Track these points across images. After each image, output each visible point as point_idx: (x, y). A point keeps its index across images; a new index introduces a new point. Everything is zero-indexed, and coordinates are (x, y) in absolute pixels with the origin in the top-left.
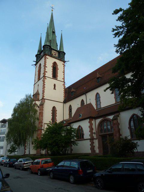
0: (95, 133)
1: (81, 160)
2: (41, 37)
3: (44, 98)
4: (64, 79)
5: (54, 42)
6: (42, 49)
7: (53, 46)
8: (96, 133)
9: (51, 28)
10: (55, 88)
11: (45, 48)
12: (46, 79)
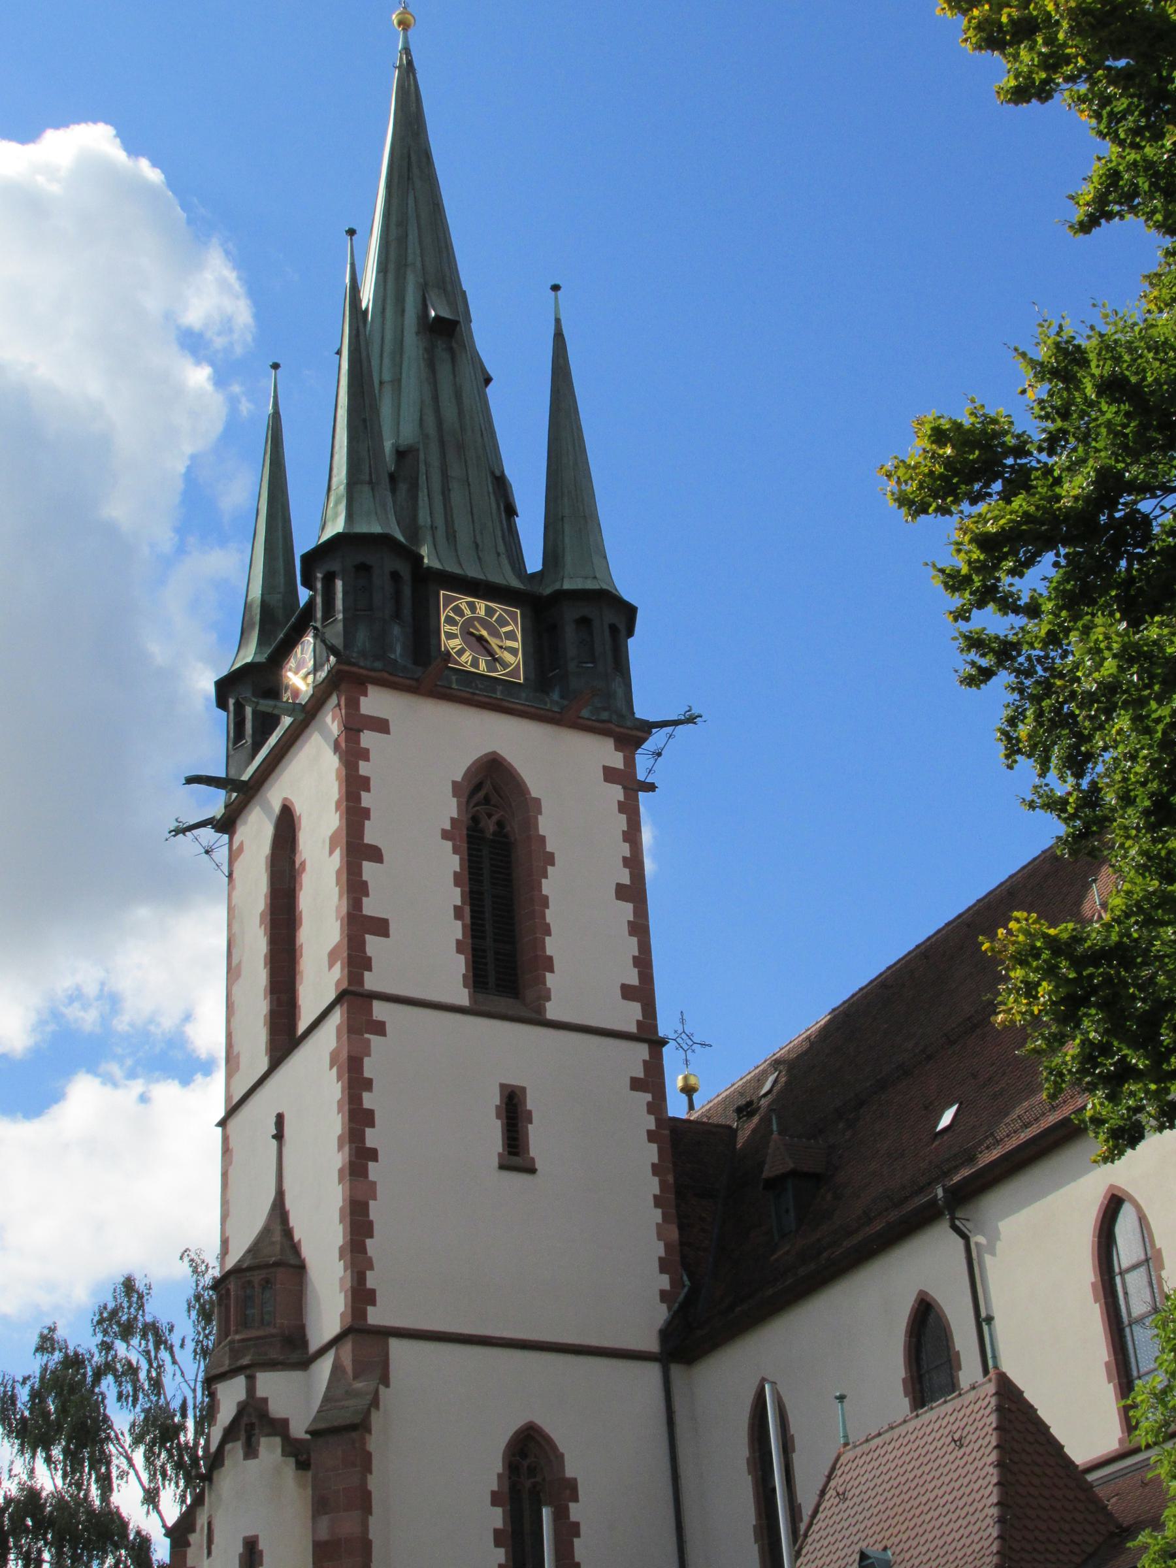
1: (421, 447)
2: (559, 337)
3: (375, 1316)
5: (455, 471)
7: (451, 536)
11: (329, 580)
12: (379, 1028)
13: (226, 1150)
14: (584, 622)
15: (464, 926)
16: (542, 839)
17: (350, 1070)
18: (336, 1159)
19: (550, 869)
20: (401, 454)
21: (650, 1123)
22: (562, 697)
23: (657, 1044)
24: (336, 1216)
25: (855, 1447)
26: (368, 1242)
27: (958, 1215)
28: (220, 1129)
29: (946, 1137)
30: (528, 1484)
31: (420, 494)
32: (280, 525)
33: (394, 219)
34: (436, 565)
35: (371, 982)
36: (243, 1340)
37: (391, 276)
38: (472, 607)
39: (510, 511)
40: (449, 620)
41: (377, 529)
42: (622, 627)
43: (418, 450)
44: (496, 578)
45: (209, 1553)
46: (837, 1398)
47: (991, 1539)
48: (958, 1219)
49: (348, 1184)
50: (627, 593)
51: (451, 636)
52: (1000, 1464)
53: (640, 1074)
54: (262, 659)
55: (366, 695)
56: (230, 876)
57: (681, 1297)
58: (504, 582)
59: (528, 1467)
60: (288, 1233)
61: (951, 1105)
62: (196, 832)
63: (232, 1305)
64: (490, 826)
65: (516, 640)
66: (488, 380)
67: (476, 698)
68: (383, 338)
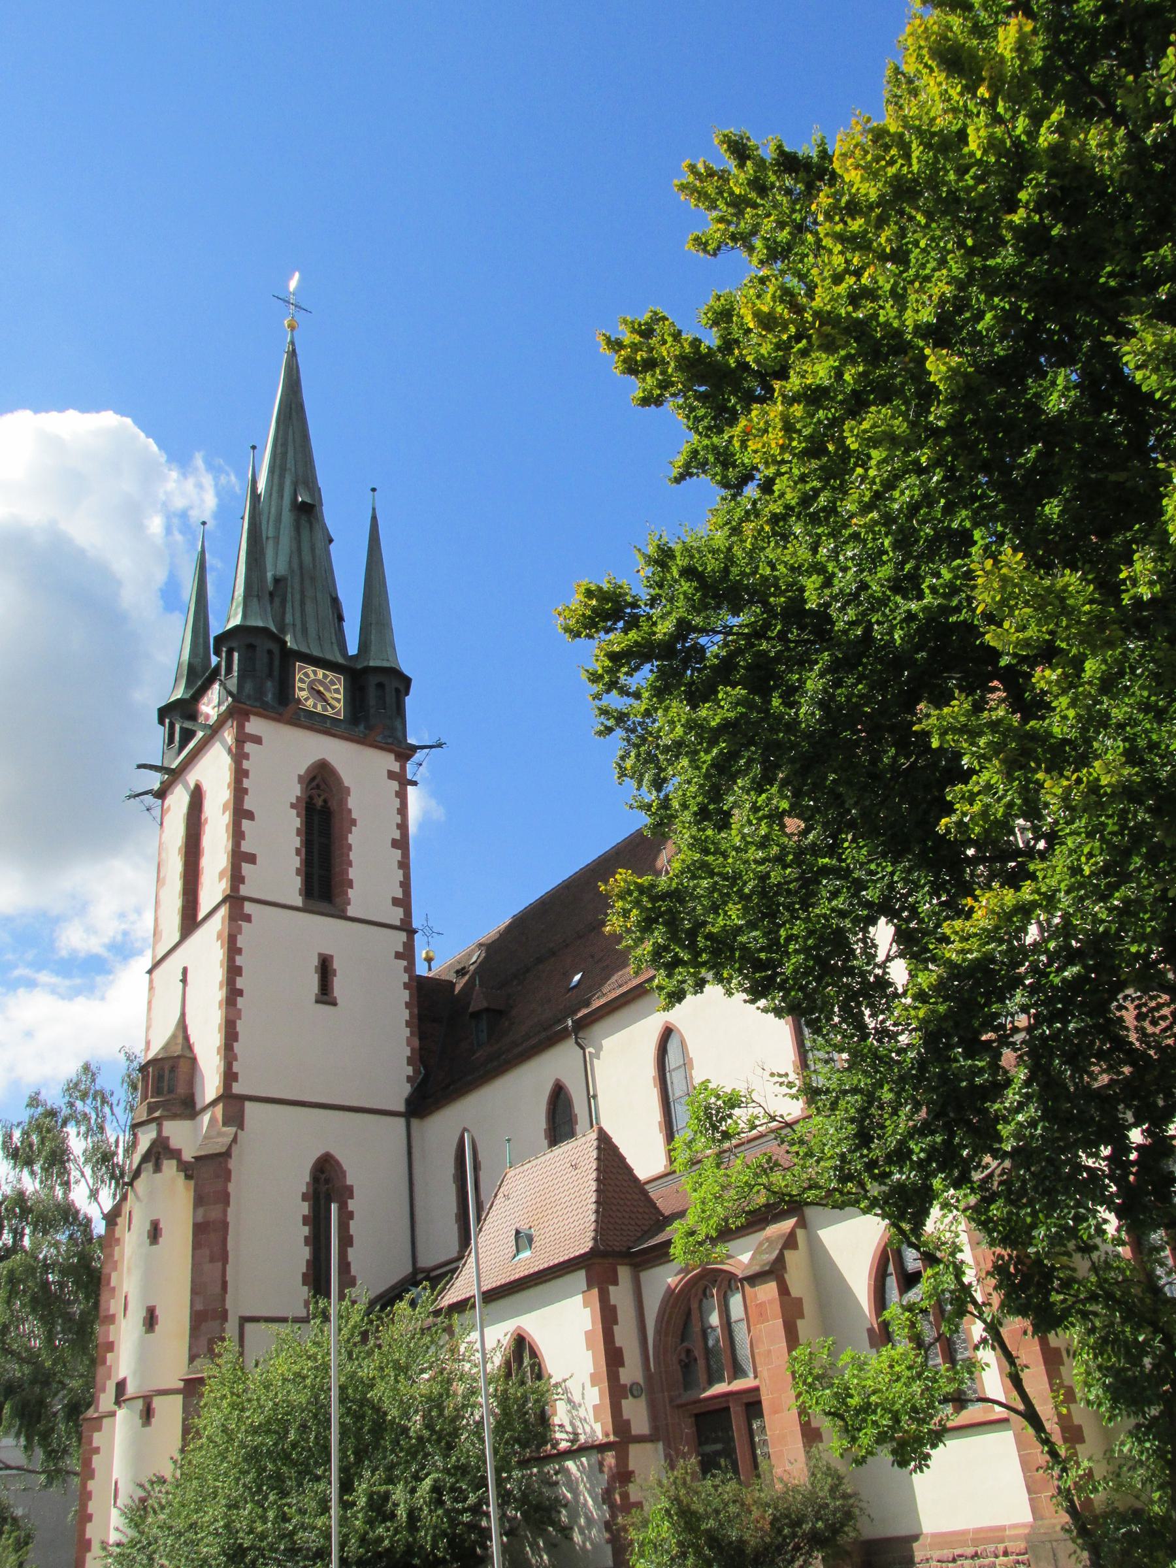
3: (237, 1088)
4: (404, 902)
7: (305, 630)
8: (651, 1388)
10: (325, 994)
12: (248, 918)
13: (151, 988)
14: (380, 686)
16: (350, 811)
18: (219, 995)
23: (411, 932)
33: (280, 442)
35: (244, 891)
38: (315, 673)
39: (341, 618)
40: (301, 681)
41: (260, 624)
42: (402, 688)
44: (329, 657)
50: (406, 670)
51: (301, 689)
52: (598, 1180)
53: (401, 950)
60: (186, 1038)
64: (319, 802)
66: (331, 541)
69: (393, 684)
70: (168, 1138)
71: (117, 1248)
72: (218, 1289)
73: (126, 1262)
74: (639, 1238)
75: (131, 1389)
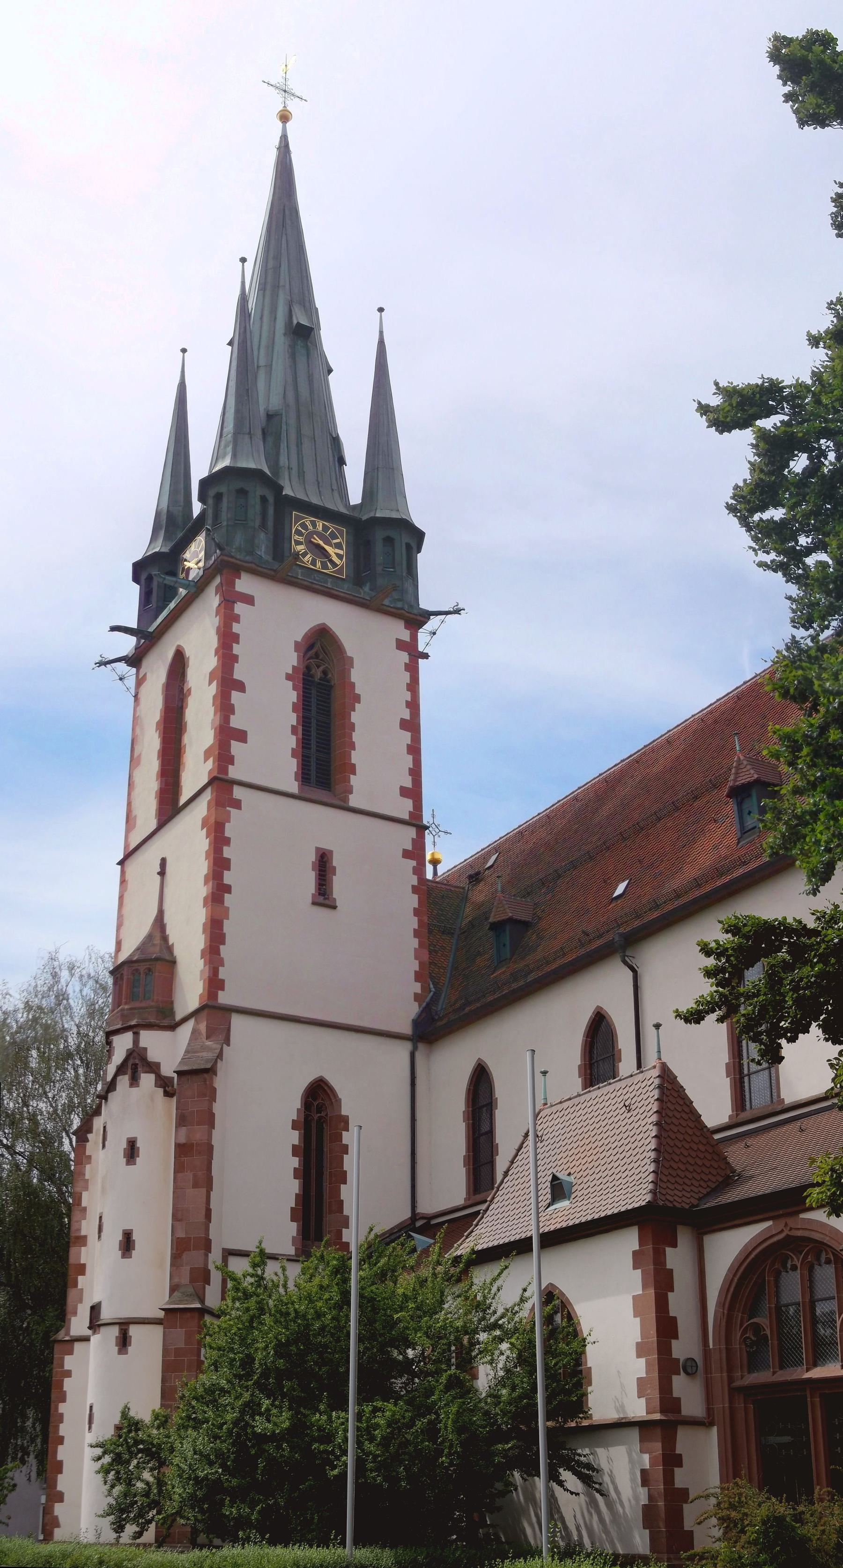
0: (689, 1368)
3: (224, 998)
4: (414, 792)
5: (306, 430)
6: (197, 508)
7: (301, 474)
9: (276, 287)
11: (219, 497)
12: (237, 804)
13: (123, 881)
14: (389, 541)
15: (297, 739)
16: (353, 685)
17: (216, 831)
18: (202, 890)
19: (357, 705)
20: (270, 417)
21: (414, 881)
22: (371, 590)
23: (422, 829)
24: (200, 929)
25: (552, 1106)
26: (222, 947)
27: (627, 954)
28: (119, 867)
29: (619, 901)
30: (316, 1117)
31: (282, 445)
32: (183, 460)
33: (271, 255)
34: (291, 494)
35: (234, 772)
36: (131, 1009)
37: (268, 292)
38: (314, 524)
39: (342, 461)
40: (298, 533)
41: (252, 465)
42: (414, 545)
43: (282, 414)
44: (330, 505)
45: (104, 1146)
46: (542, 1073)
47: (647, 1173)
48: (628, 956)
49: (210, 908)
50: (418, 521)
51: (298, 543)
52: (658, 1124)
53: (410, 848)
54: (166, 550)
55: (240, 578)
56: (136, 696)
57: (428, 999)
58: (336, 509)
59: (317, 1105)
60: (165, 938)
61: (624, 881)
62: (114, 665)
63: (124, 985)
64: (318, 674)
65: (343, 550)
66: (330, 371)
67: (314, 586)
68: (260, 336)
69: (403, 539)
70: (145, 1049)
71: (88, 1167)
72: (202, 1218)
73: (100, 1181)
74: (705, 1196)
75: (106, 1314)
